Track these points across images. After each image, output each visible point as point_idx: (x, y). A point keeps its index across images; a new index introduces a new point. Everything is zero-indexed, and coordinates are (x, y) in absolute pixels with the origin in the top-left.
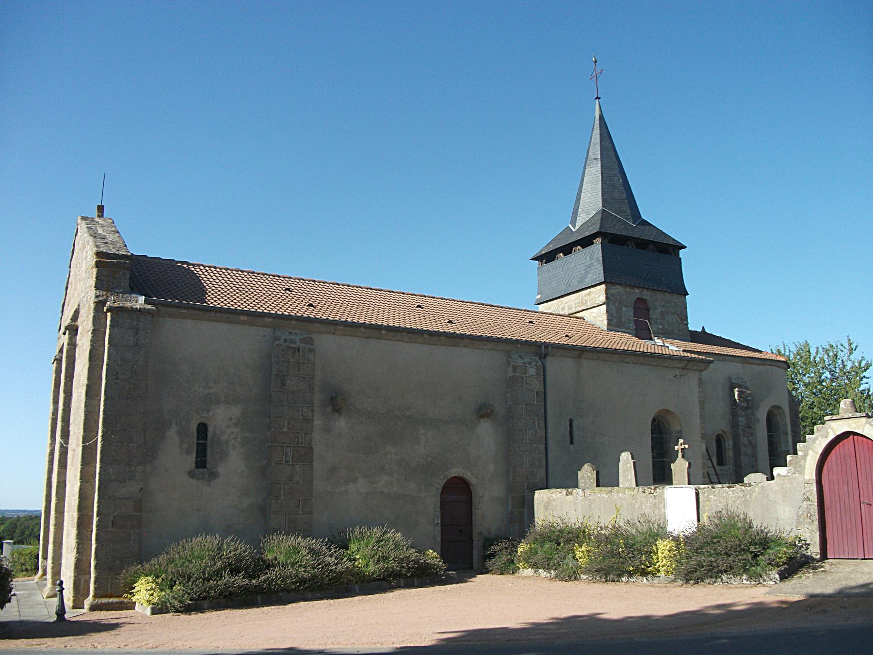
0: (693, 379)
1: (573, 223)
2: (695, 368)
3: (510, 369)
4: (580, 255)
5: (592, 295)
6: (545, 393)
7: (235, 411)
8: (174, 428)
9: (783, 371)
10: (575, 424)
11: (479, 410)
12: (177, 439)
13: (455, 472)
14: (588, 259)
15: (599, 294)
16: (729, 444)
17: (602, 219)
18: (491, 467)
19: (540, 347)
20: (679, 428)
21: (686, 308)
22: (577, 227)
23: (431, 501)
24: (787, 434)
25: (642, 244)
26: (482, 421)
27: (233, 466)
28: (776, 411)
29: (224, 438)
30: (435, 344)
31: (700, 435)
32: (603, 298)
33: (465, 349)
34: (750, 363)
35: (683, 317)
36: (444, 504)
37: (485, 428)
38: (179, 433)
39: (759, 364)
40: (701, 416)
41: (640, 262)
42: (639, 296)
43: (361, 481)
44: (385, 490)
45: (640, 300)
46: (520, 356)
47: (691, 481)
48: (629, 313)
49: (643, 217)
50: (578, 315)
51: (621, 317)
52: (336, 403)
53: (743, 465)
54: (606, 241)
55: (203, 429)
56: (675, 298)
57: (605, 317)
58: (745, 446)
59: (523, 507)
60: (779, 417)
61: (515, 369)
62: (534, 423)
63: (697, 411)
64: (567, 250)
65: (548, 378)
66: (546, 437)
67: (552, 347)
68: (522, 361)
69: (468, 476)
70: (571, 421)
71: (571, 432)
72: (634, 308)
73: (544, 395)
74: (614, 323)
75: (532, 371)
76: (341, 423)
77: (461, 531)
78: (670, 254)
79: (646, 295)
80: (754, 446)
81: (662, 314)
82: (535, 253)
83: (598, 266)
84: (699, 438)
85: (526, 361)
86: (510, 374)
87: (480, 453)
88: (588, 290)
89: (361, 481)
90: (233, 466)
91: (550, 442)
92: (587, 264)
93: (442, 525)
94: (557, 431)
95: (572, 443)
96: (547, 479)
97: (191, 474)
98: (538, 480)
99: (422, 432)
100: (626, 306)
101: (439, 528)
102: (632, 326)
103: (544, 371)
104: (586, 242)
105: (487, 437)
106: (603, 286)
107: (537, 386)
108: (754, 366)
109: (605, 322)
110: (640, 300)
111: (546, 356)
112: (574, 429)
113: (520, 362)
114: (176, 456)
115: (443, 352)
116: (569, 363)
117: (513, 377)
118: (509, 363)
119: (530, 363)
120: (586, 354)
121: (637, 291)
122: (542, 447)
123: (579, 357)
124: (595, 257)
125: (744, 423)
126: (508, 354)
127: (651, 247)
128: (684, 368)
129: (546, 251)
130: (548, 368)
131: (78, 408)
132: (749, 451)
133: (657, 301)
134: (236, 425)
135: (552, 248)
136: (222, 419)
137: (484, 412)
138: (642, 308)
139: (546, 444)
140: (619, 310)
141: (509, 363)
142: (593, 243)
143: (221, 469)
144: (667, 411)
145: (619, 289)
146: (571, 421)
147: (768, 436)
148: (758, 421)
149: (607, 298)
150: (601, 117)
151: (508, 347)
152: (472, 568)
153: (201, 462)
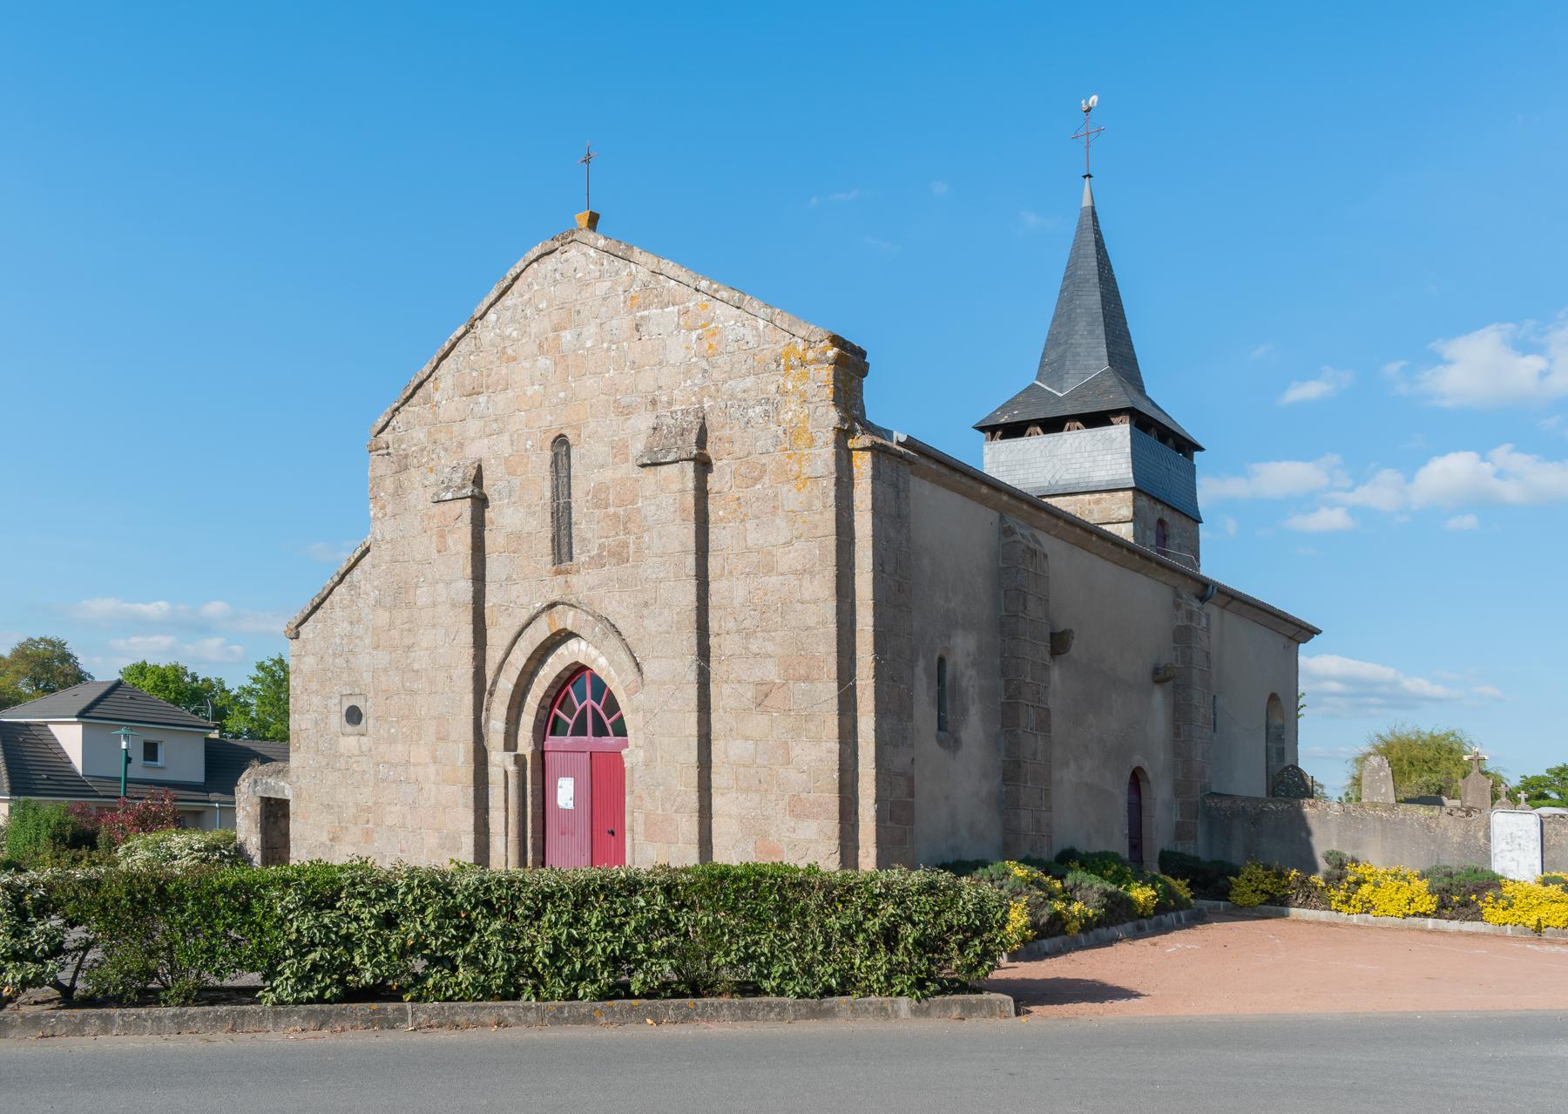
5: (1104, 505)
79: (1167, 515)
106: (1130, 493)
120: (1235, 604)
133: (1175, 523)
141: (1177, 606)
145: (1144, 501)
149: (1135, 514)
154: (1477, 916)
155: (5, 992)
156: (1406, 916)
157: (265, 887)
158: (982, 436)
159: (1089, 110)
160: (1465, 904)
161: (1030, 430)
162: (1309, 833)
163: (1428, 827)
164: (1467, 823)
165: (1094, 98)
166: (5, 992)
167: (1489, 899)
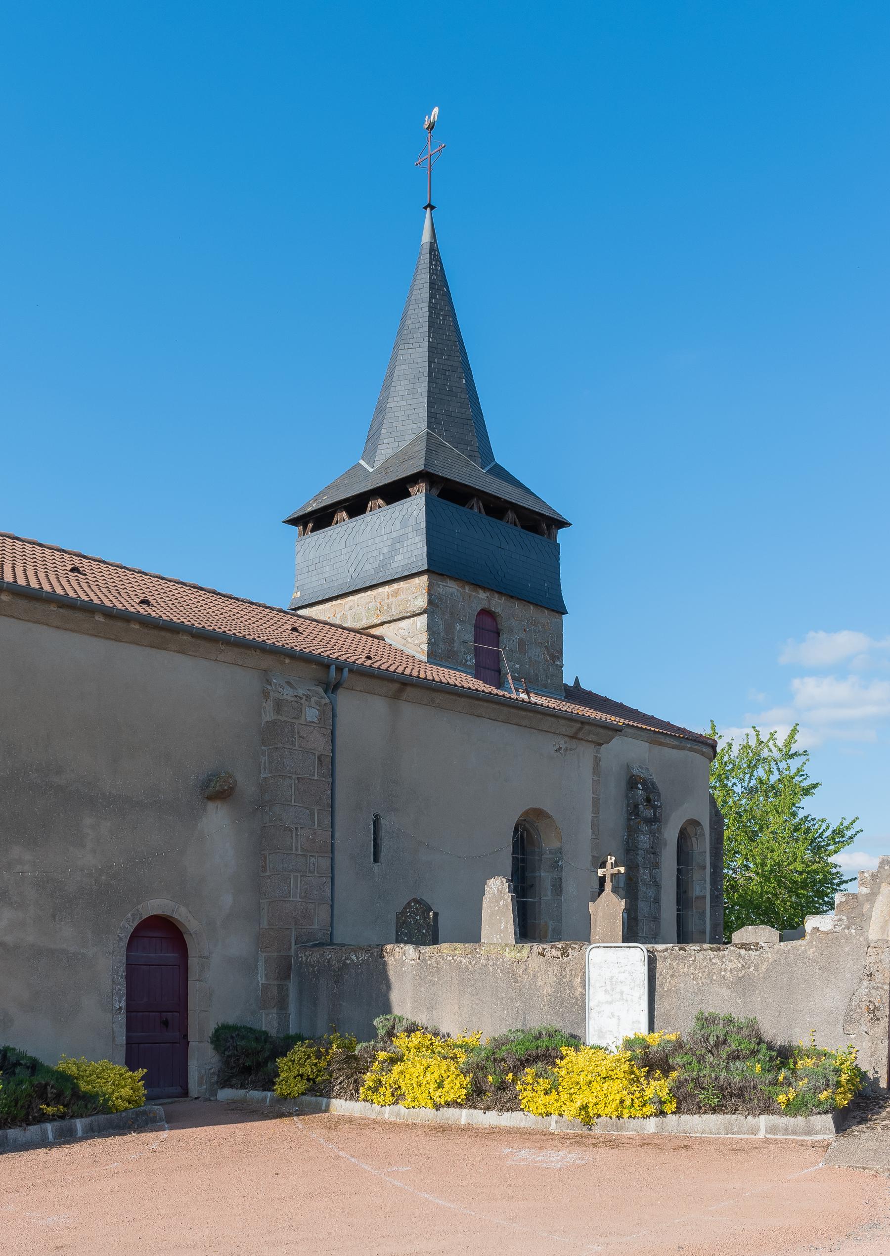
0: (586, 753)
1: (369, 453)
2: (591, 737)
3: (269, 705)
4: (381, 519)
5: (402, 596)
6: (333, 759)
9: (708, 761)
10: (384, 823)
11: (206, 784)
13: (155, 906)
14: (398, 525)
15: (415, 593)
17: (429, 450)
18: (227, 900)
19: (328, 667)
20: (556, 845)
21: (561, 637)
22: (377, 465)
23: (107, 965)
24: (704, 868)
25: (496, 508)
26: (211, 806)
28: (690, 830)
30: (117, 639)
32: (421, 602)
33: (179, 658)
34: (661, 744)
35: (556, 654)
36: (132, 970)
37: (217, 820)
39: (674, 747)
40: (593, 825)
41: (494, 542)
42: (485, 605)
45: (486, 613)
46: (288, 683)
47: (693, 925)
48: (465, 633)
49: (498, 460)
50: (374, 631)
51: (452, 640)
53: (640, 917)
54: (435, 492)
56: (544, 617)
57: (424, 638)
58: (645, 884)
59: (288, 977)
60: (694, 839)
61: (279, 705)
62: (312, 814)
63: (589, 815)
64: (356, 506)
65: (338, 733)
66: (332, 845)
67: (351, 671)
68: (291, 692)
69: (182, 914)
71: (375, 840)
72: (476, 627)
73: (329, 763)
74: (434, 656)
75: (311, 714)
77: (166, 1023)
78: (542, 534)
79: (498, 604)
80: (658, 886)
81: (521, 642)
82: (285, 518)
83: (418, 539)
85: (300, 692)
86: (269, 716)
87: (209, 871)
88: (395, 586)
91: (338, 857)
92: (394, 535)
93: (128, 1011)
94: (351, 835)
95: (376, 859)
96: (332, 925)
98: (316, 926)
99: (88, 821)
100: (462, 622)
101: (122, 1018)
102: (471, 660)
103: (334, 716)
104: (394, 492)
105: (219, 833)
106: (424, 578)
107: (318, 742)
108: (667, 750)
109: (425, 647)
110: (486, 613)
111: (336, 687)
112: (382, 834)
113: (288, 693)
115: (134, 660)
116: (378, 705)
117: (274, 723)
118: (266, 695)
119: (308, 698)
120: (410, 692)
121: (482, 595)
122: (325, 863)
123: (396, 696)
124: (412, 521)
125: (647, 845)
126: (266, 673)
127: (511, 515)
128: (573, 737)
129: (315, 506)
130: (339, 711)
132: (651, 893)
133: (514, 616)
135: (326, 501)
137: (217, 790)
138: (488, 626)
139: (332, 859)
140: (450, 628)
141: (266, 695)
142: (408, 495)
144: (539, 813)
145: (451, 588)
147: (678, 870)
148: (666, 844)
149: (430, 602)
150: (434, 250)
151: (268, 662)
152: (185, 1093)
154: (513, 1104)
155: (887, 1174)
156: (437, 1107)
157: (355, 1081)
158: (296, 530)
159: (431, 127)
160: (502, 1087)
161: (337, 516)
162: (389, 987)
163: (514, 975)
164: (563, 967)
165: (436, 110)
166: (887, 1174)
167: (529, 1079)
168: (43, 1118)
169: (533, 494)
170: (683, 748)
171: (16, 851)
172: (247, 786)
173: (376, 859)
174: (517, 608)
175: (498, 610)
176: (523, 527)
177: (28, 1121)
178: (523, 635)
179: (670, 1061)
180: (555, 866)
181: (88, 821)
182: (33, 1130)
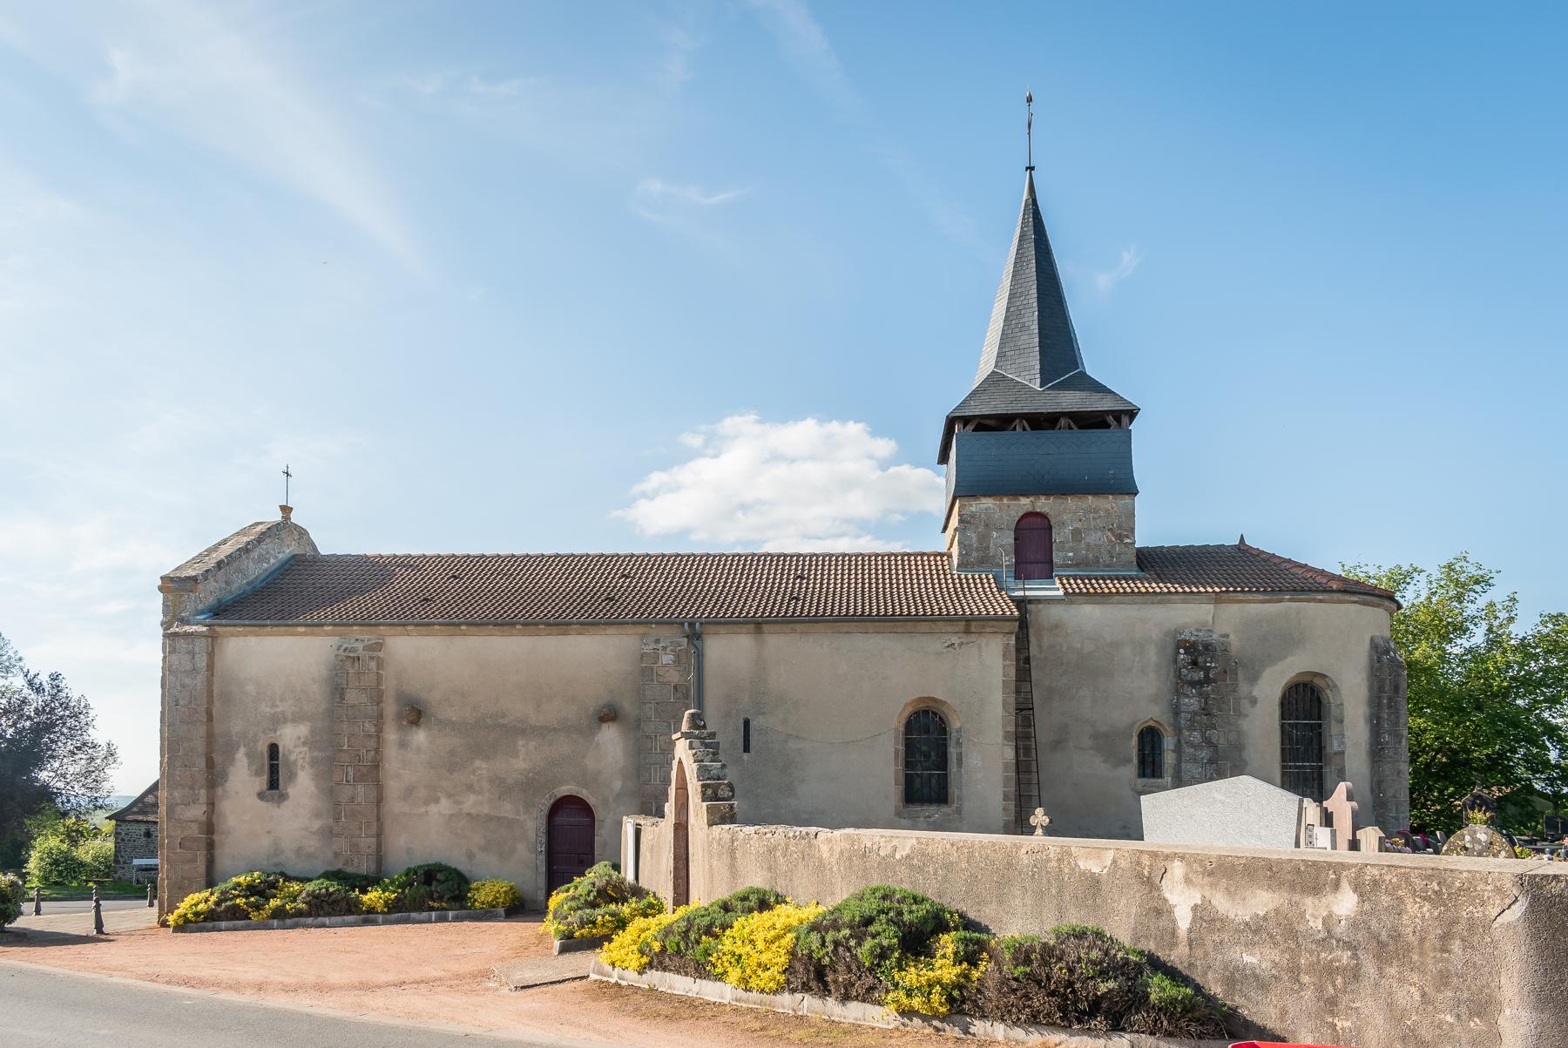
7: (303, 730)
8: (242, 751)
12: (245, 761)
13: (565, 790)
16: (1168, 743)
26: (605, 726)
27: (303, 786)
29: (293, 758)
31: (1001, 733)
38: (248, 755)
41: (1043, 443)
43: (444, 801)
44: (473, 811)
52: (415, 713)
55: (274, 750)
58: (1192, 745)
70: (747, 723)
76: (420, 736)
79: (1043, 504)
84: (1000, 739)
89: (444, 801)
90: (303, 786)
95: (747, 749)
97: (261, 796)
101: (543, 857)
114: (243, 779)
127: (1063, 422)
131: (986, 363)
134: (304, 744)
136: (291, 737)
137: (609, 715)
143: (291, 791)
146: (747, 723)
153: (273, 784)
168: (432, 909)
169: (1111, 392)
170: (1281, 601)
171: (478, 763)
172: (628, 706)
173: (747, 749)
174: (1071, 502)
175: (1045, 510)
176: (1080, 428)
177: (420, 909)
178: (1078, 525)
179: (1321, 936)
180: (959, 744)
181: (44, 776)
182: (425, 914)
